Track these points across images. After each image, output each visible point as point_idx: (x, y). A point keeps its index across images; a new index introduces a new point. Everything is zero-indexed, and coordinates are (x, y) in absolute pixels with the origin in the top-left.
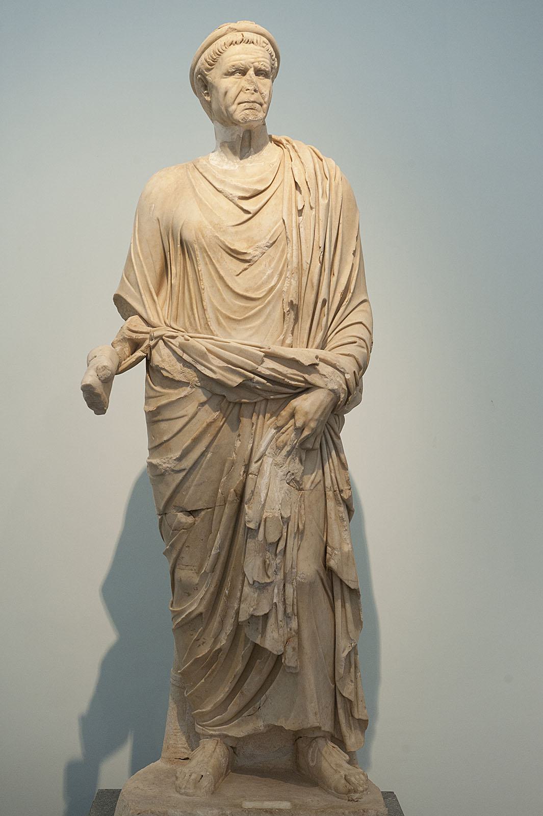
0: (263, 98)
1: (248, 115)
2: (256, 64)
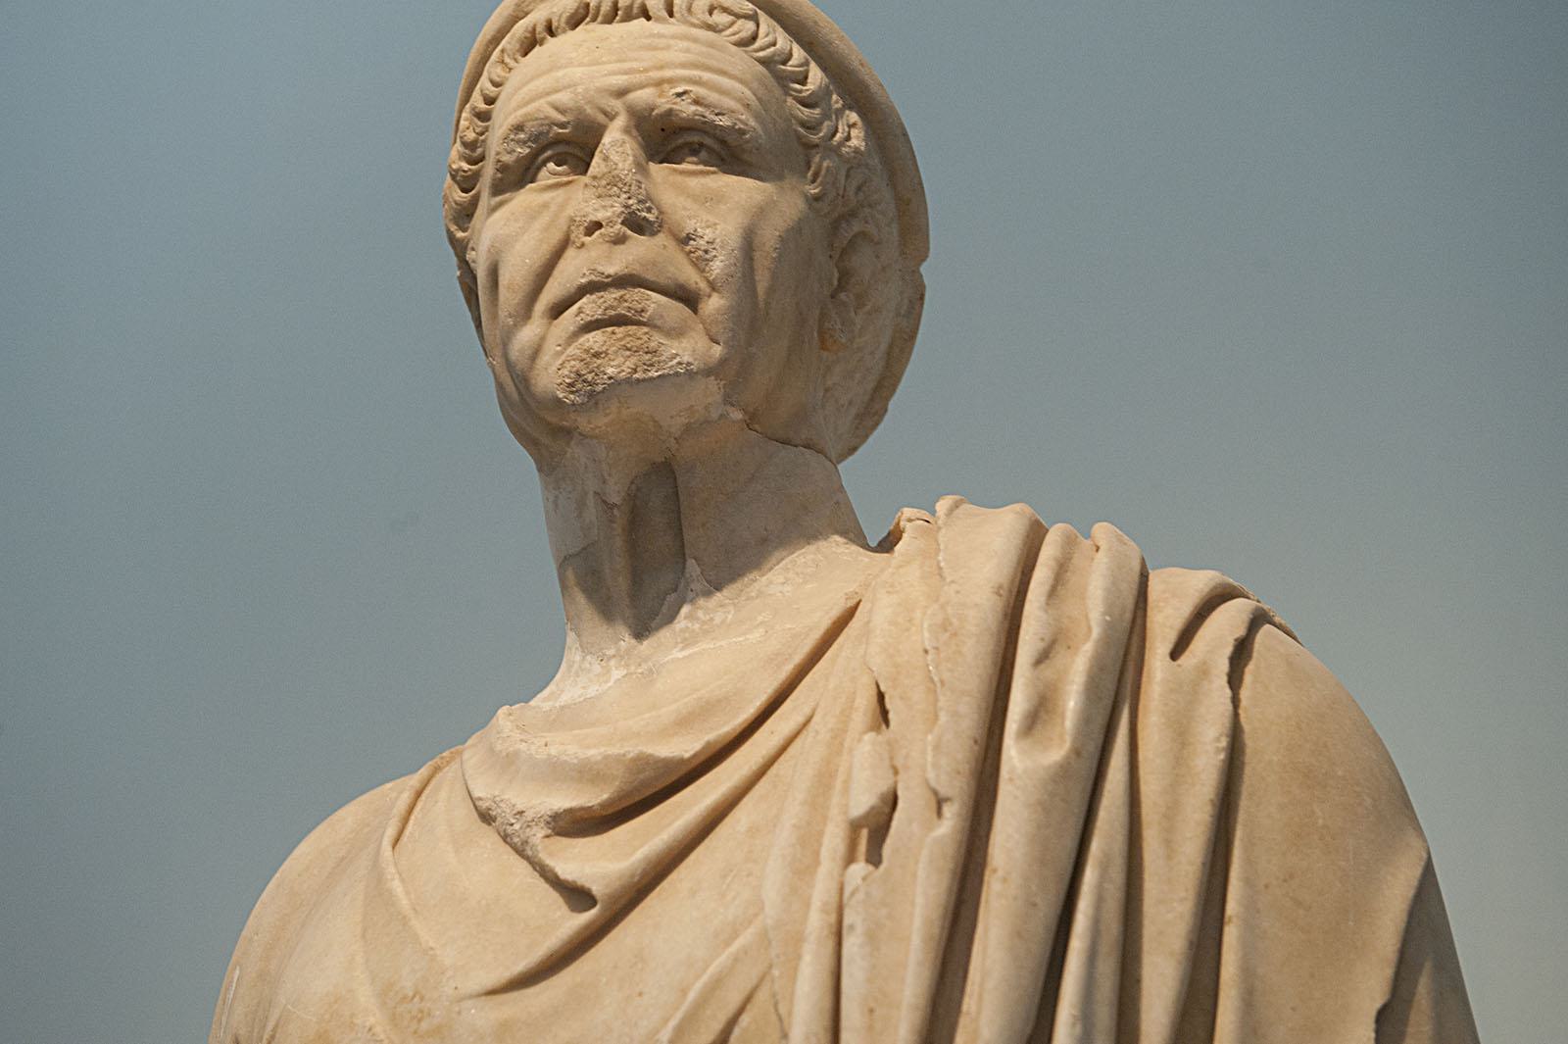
0: (700, 263)
1: (597, 355)
2: (642, 96)
